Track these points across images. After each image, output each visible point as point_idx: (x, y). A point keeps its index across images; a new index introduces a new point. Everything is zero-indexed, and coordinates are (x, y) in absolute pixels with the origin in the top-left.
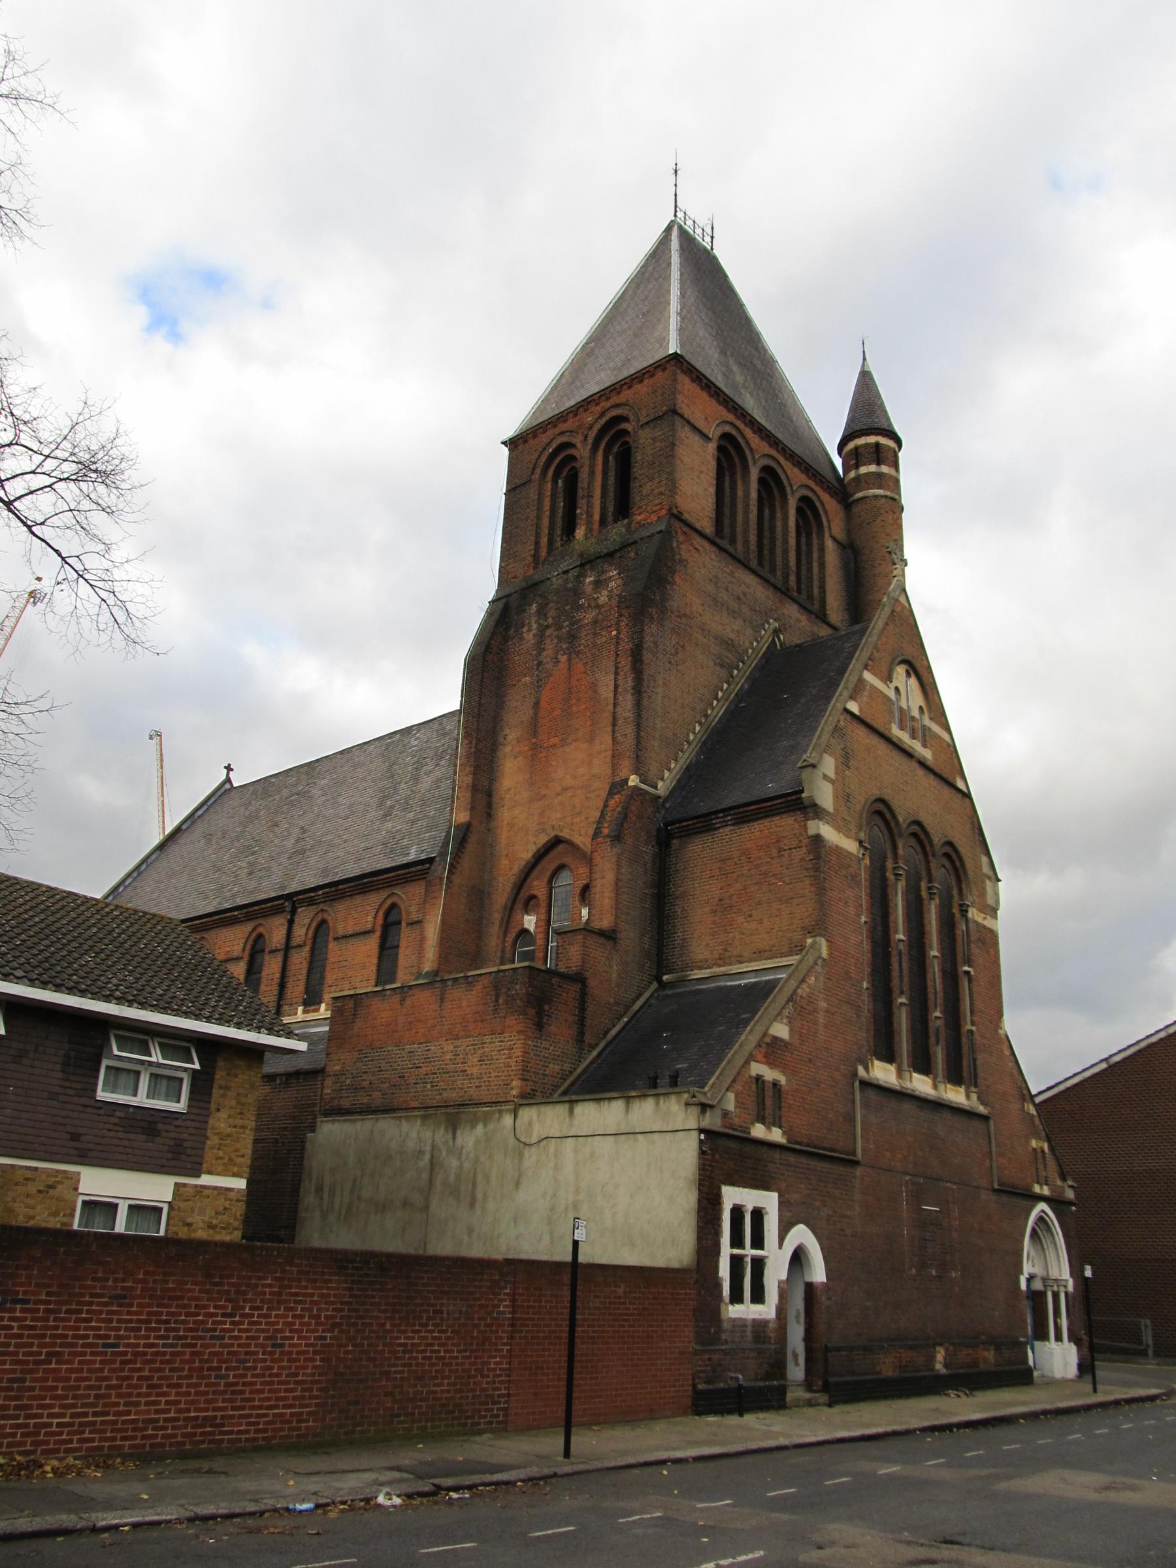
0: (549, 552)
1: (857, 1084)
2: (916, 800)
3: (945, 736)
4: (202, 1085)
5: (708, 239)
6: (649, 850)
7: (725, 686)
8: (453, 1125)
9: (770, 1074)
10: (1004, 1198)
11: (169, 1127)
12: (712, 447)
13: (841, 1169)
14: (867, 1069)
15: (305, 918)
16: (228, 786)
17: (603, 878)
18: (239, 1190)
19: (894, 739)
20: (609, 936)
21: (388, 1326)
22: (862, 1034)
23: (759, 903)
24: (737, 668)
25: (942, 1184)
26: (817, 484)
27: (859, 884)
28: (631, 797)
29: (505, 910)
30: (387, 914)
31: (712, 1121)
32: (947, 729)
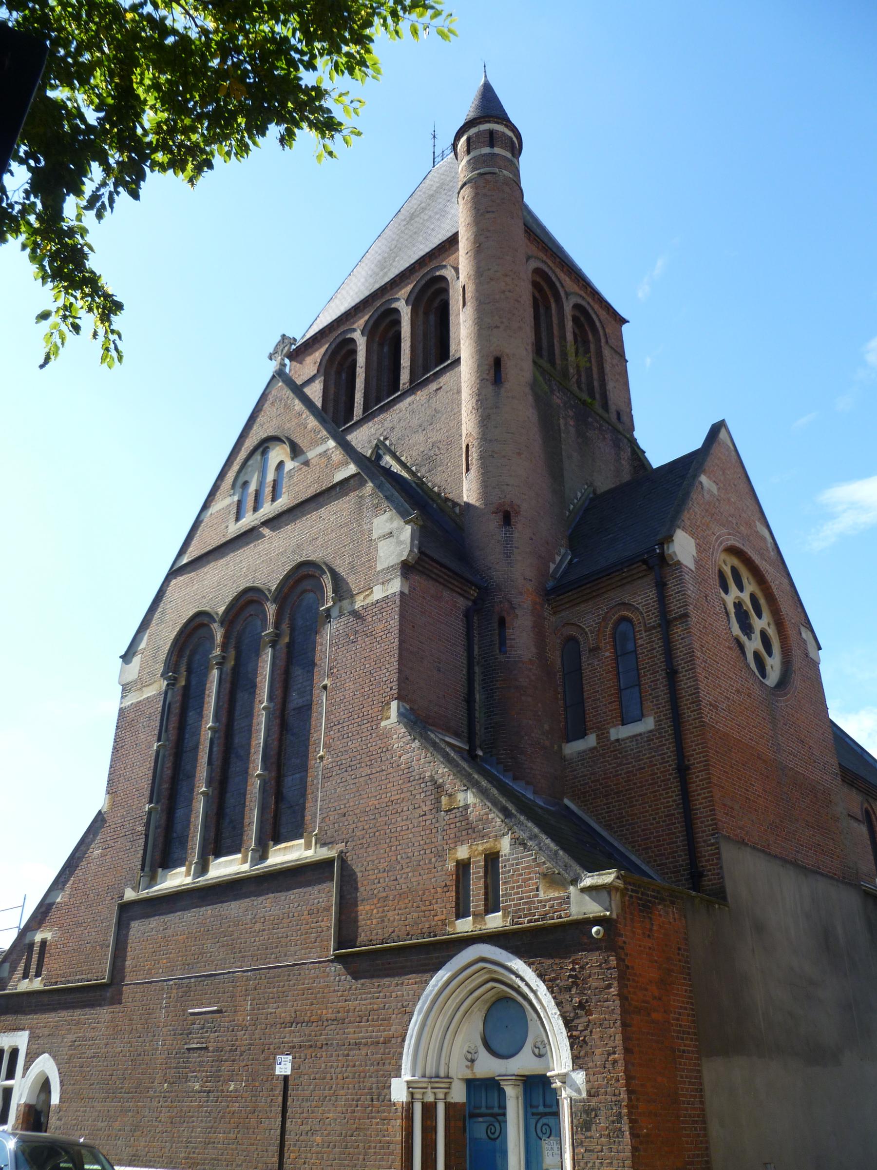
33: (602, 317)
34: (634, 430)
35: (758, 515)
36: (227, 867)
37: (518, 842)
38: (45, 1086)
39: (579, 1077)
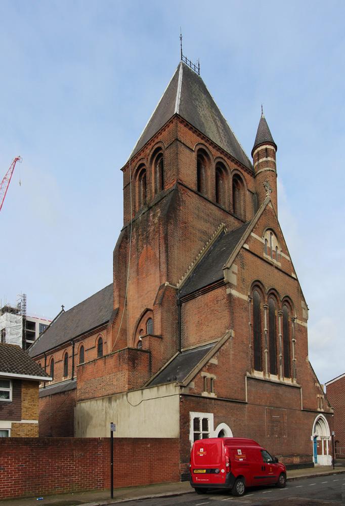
1: (246, 378)
2: (272, 280)
3: (288, 258)
4: (17, 395)
5: (197, 70)
6: (174, 308)
7: (203, 248)
8: (110, 400)
9: (209, 375)
10: (306, 413)
11: (6, 406)
12: (194, 155)
13: (240, 405)
14: (251, 373)
15: (77, 345)
16: (63, 312)
17: (157, 318)
18: (36, 424)
19: (265, 259)
20: (160, 337)
21: (50, 460)
22: (248, 361)
23: (211, 321)
24: (208, 241)
25: (280, 409)
27: (248, 311)
28: (166, 289)
29: (133, 334)
30: (99, 341)
31: (183, 391)
32: (289, 255)
33: (245, 175)
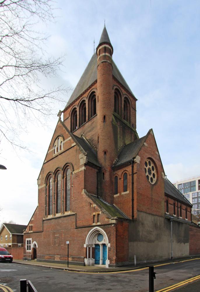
0: (88, 119)
26: (128, 94)
33: (131, 100)
34: (136, 128)
35: (156, 150)
36: (58, 215)
37: (103, 212)
38: (35, 245)
39: (110, 244)
